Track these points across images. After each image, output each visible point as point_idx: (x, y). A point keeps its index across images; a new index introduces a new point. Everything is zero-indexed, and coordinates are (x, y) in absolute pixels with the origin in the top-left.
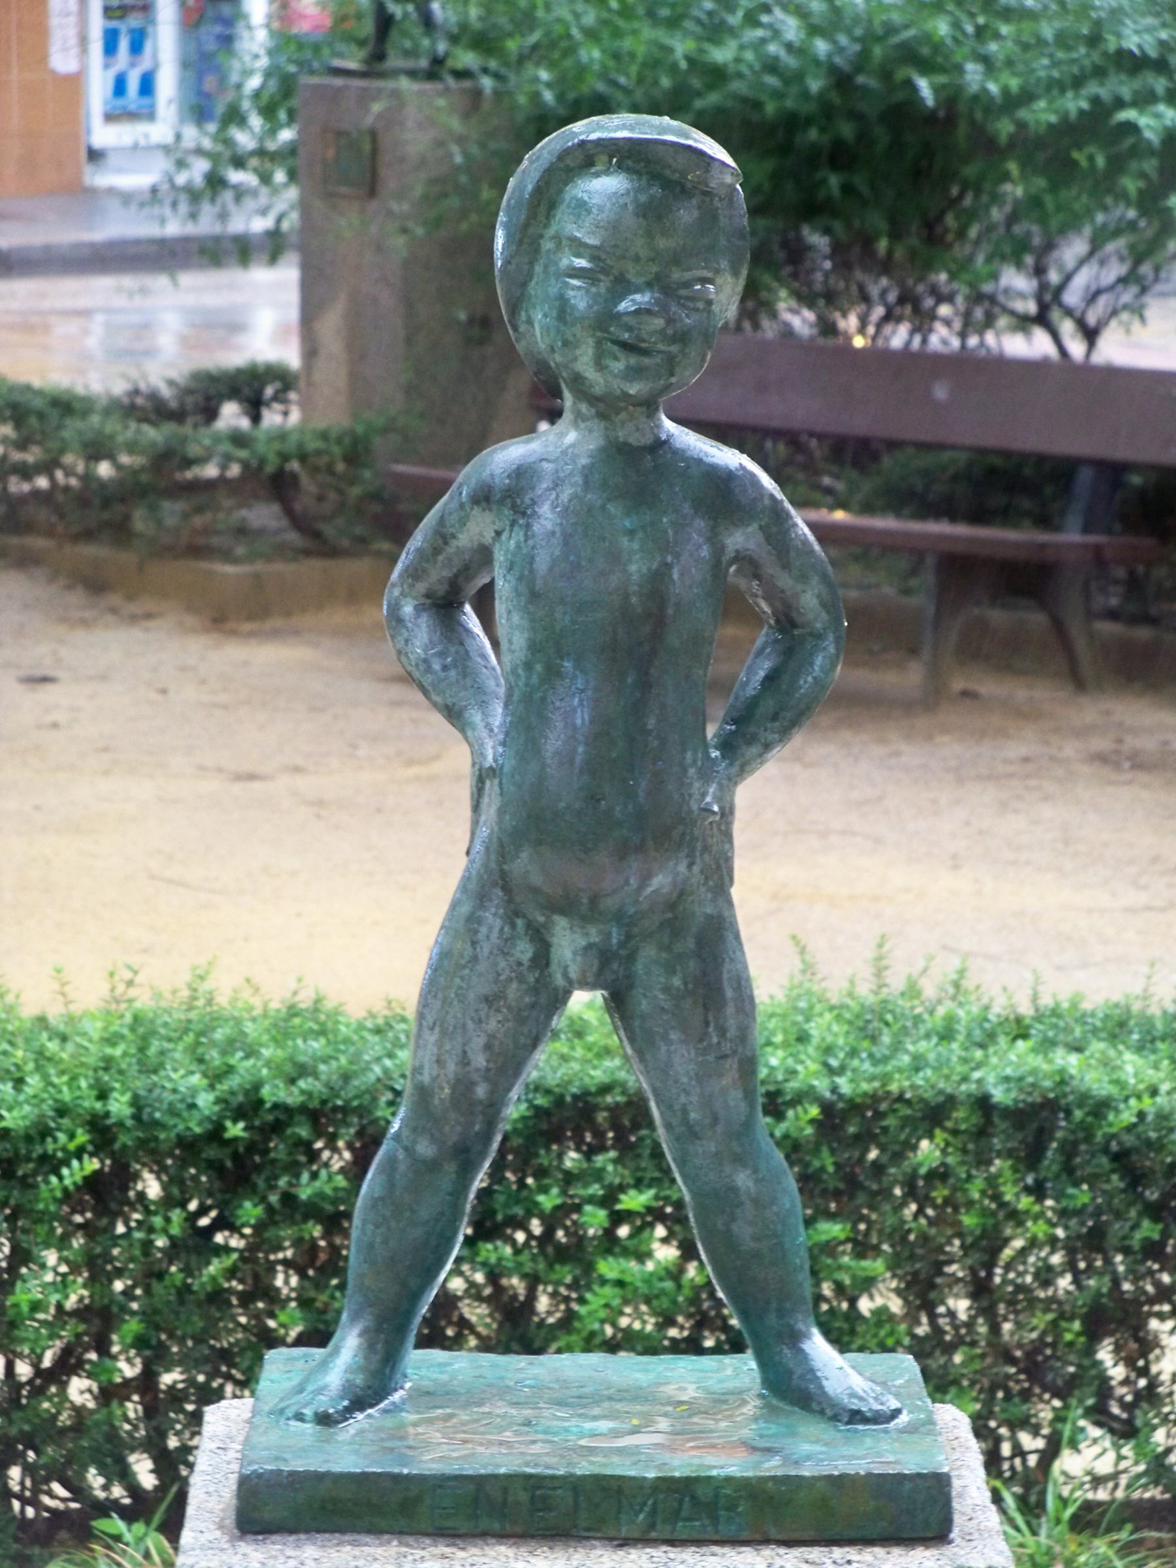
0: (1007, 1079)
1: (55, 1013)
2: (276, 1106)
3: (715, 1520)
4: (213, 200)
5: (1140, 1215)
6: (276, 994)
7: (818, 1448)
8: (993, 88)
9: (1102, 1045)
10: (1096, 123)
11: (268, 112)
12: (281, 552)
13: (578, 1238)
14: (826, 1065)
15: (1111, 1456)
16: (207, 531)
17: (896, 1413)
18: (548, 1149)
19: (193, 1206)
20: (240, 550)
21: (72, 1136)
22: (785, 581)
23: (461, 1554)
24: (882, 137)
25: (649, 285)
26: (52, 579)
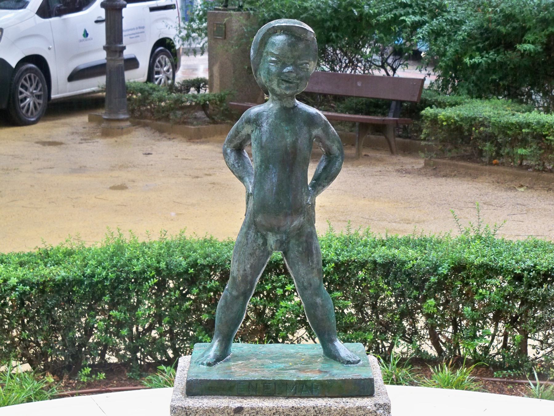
0: (380, 256)
1: (147, 241)
2: (201, 265)
3: (312, 392)
4: (188, 41)
5: (413, 289)
6: (201, 235)
7: (338, 371)
8: (371, 12)
9: (404, 247)
10: (395, 20)
11: (200, 19)
12: (204, 122)
13: (276, 295)
14: (336, 253)
15: (406, 348)
16: (187, 118)
17: (360, 361)
18: (268, 274)
19: (181, 288)
20: (195, 123)
21: (151, 273)
22: (328, 143)
23: (245, 401)
24: (345, 24)
25: (292, 65)
26: (152, 129)
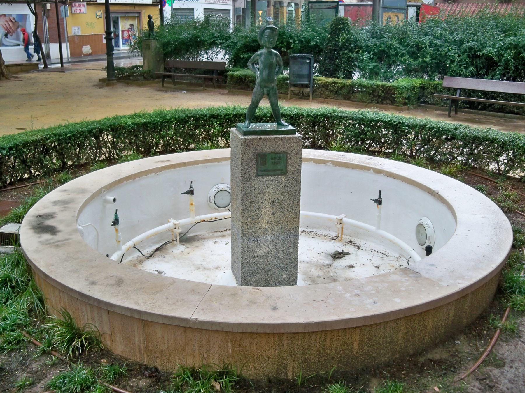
24: (195, 44)
